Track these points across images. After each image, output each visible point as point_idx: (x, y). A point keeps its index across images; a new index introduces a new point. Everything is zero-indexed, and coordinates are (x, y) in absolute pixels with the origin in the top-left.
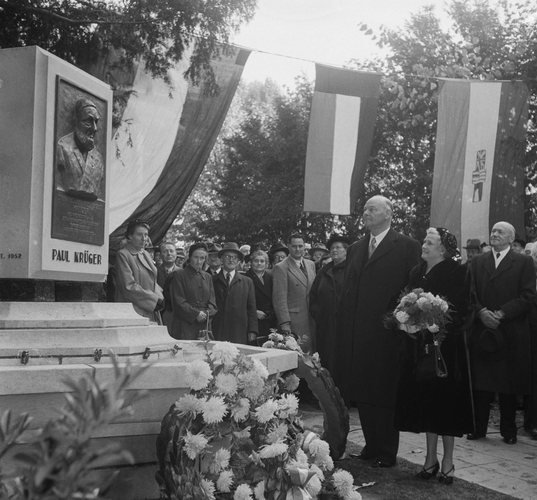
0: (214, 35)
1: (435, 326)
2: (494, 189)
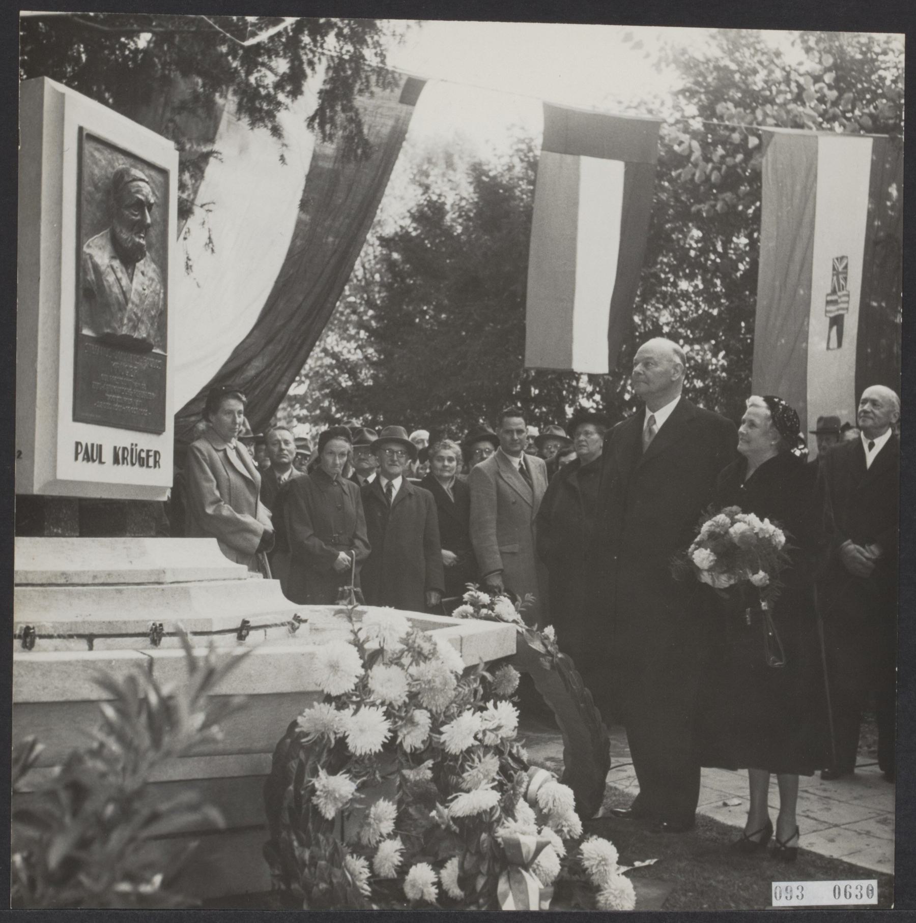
0: (360, 53)
1: (761, 574)
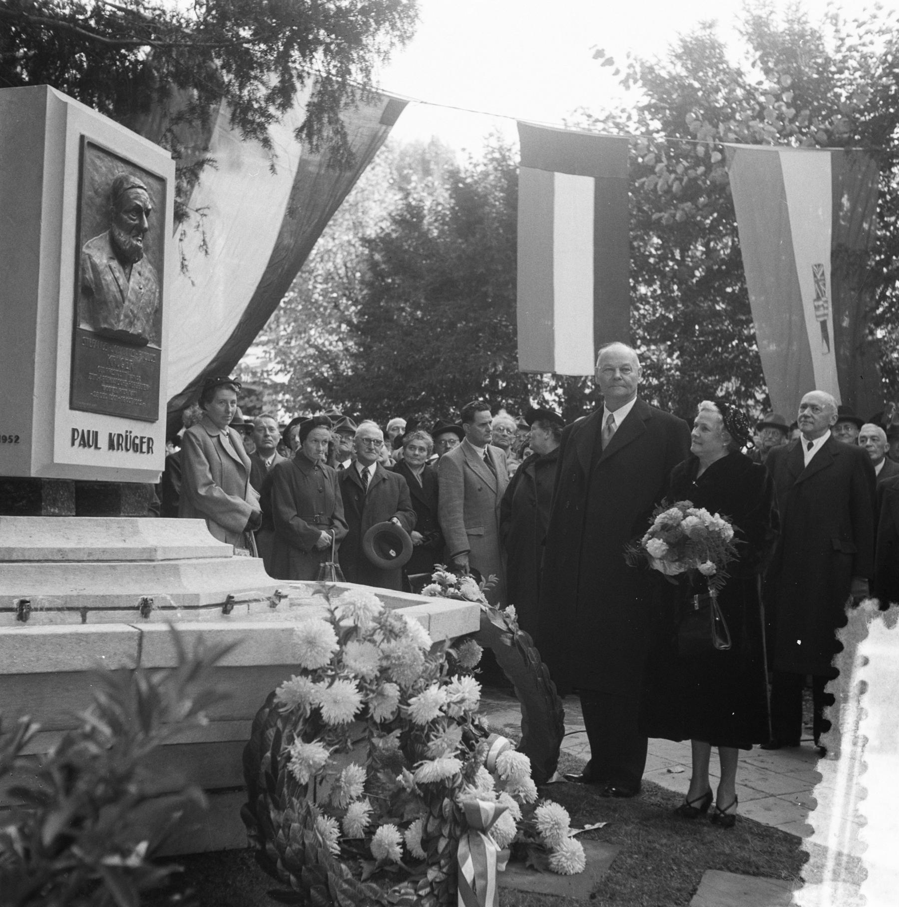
0: (347, 67)
1: (709, 564)
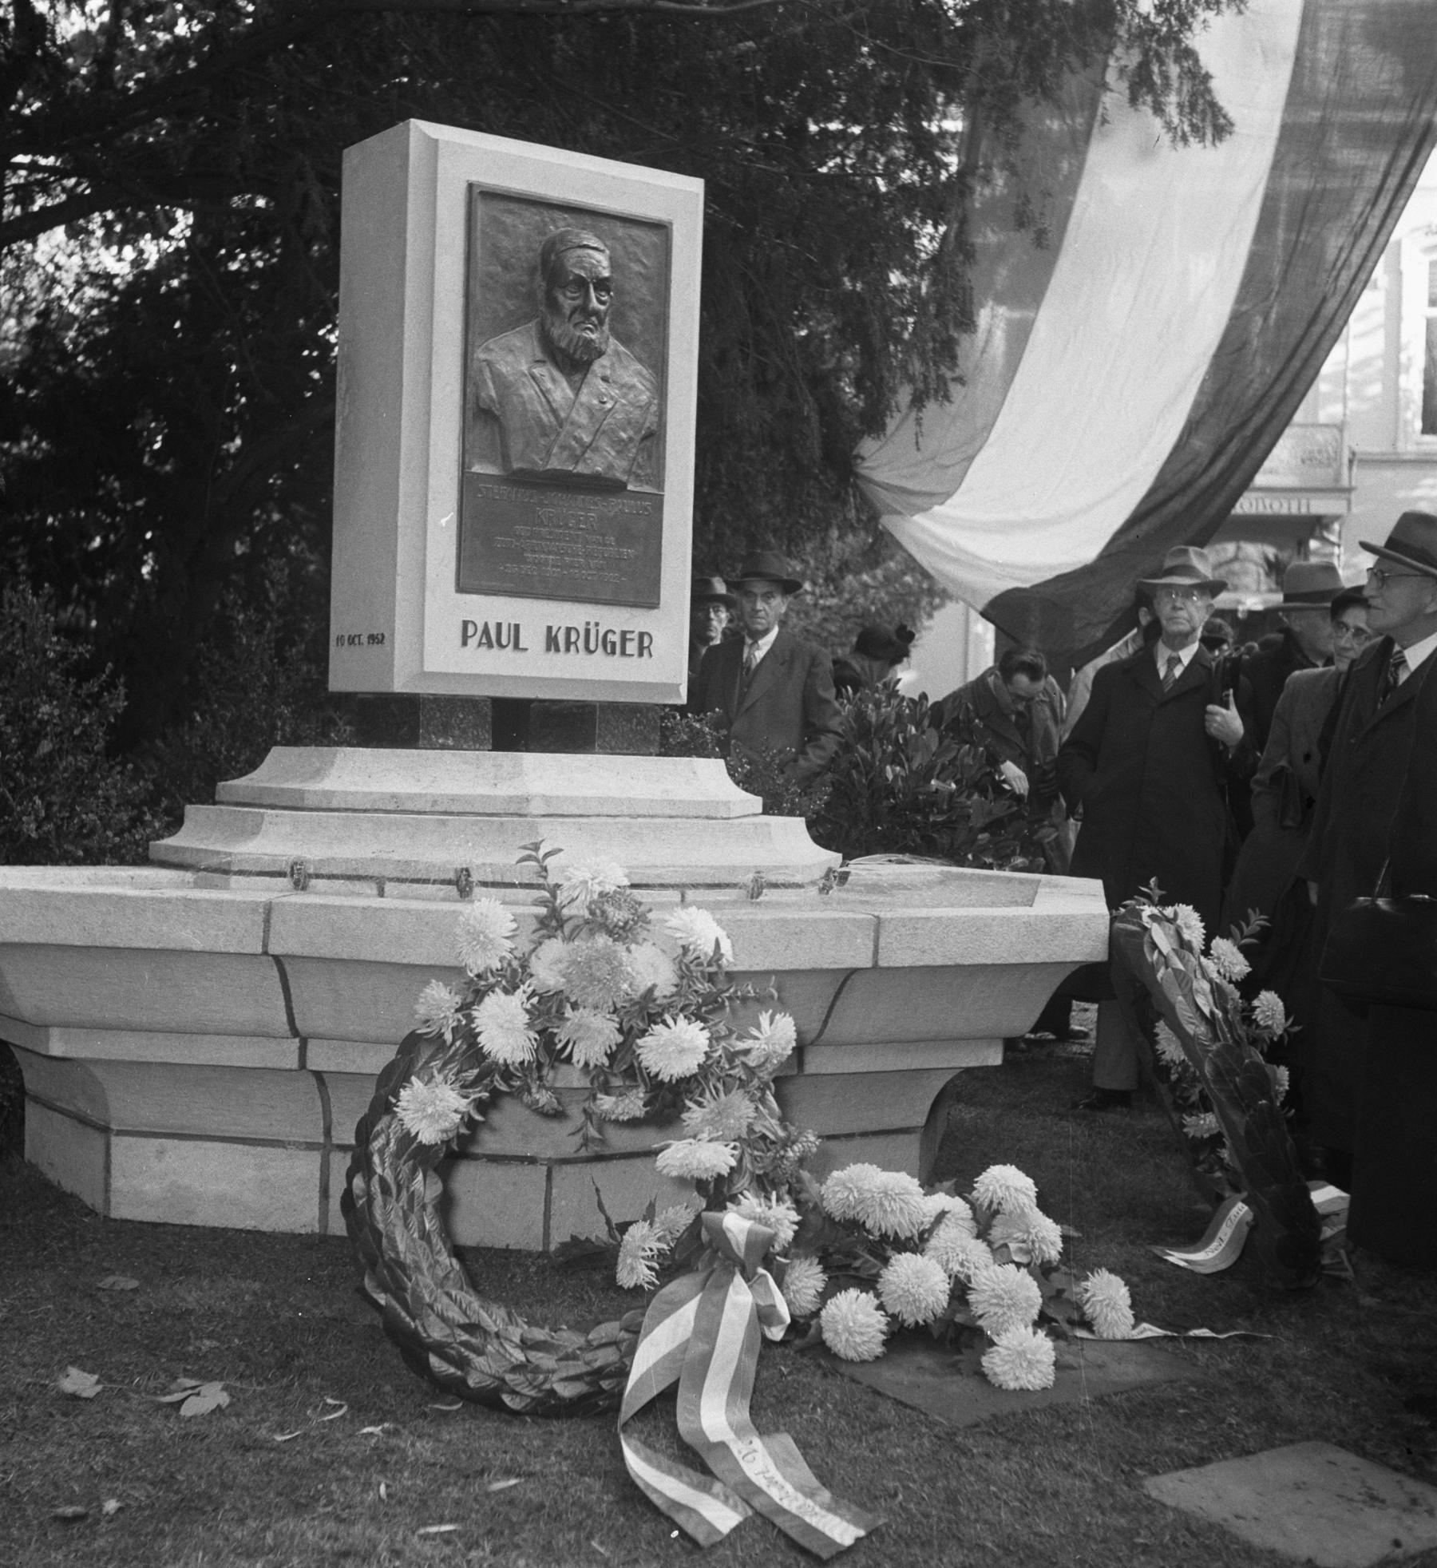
2: (323, 601)
